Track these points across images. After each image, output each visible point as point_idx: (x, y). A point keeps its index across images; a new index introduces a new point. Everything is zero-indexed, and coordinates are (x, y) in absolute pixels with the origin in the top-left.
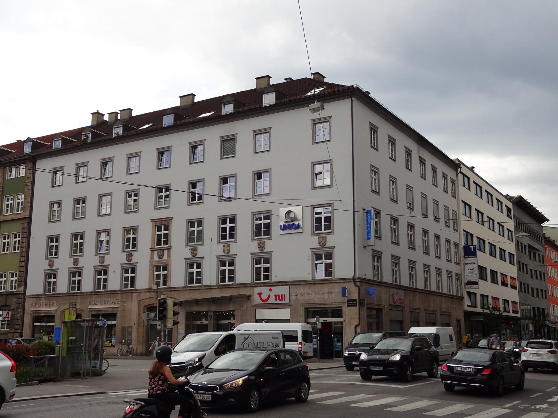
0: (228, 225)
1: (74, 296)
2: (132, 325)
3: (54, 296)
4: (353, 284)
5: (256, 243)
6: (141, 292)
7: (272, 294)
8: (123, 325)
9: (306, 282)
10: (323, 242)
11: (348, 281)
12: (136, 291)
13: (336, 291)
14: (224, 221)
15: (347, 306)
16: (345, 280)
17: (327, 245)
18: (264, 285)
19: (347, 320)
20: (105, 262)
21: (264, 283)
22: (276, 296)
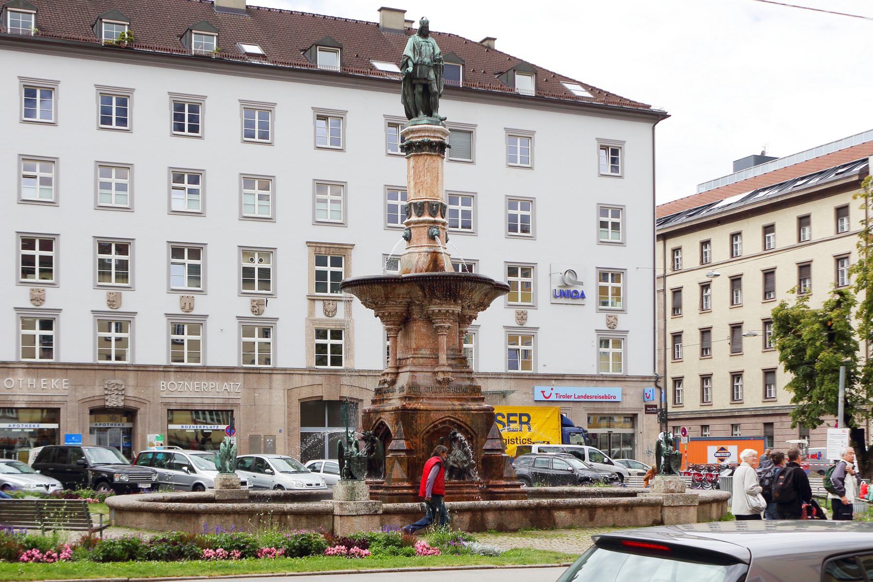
0: (37, 253)
1: (116, 372)
2: (275, 432)
3: (57, 367)
4: (652, 384)
5: (247, 300)
6: (293, 374)
7: (554, 392)
8: (254, 433)
9: (592, 377)
10: (257, 307)
11: (647, 380)
12: (283, 372)
13: (632, 393)
14: (104, 248)
15: (646, 413)
16: (644, 379)
17: (618, 328)
18: (529, 377)
19: (645, 431)
20: (195, 309)
21: (522, 375)
22: (557, 394)
